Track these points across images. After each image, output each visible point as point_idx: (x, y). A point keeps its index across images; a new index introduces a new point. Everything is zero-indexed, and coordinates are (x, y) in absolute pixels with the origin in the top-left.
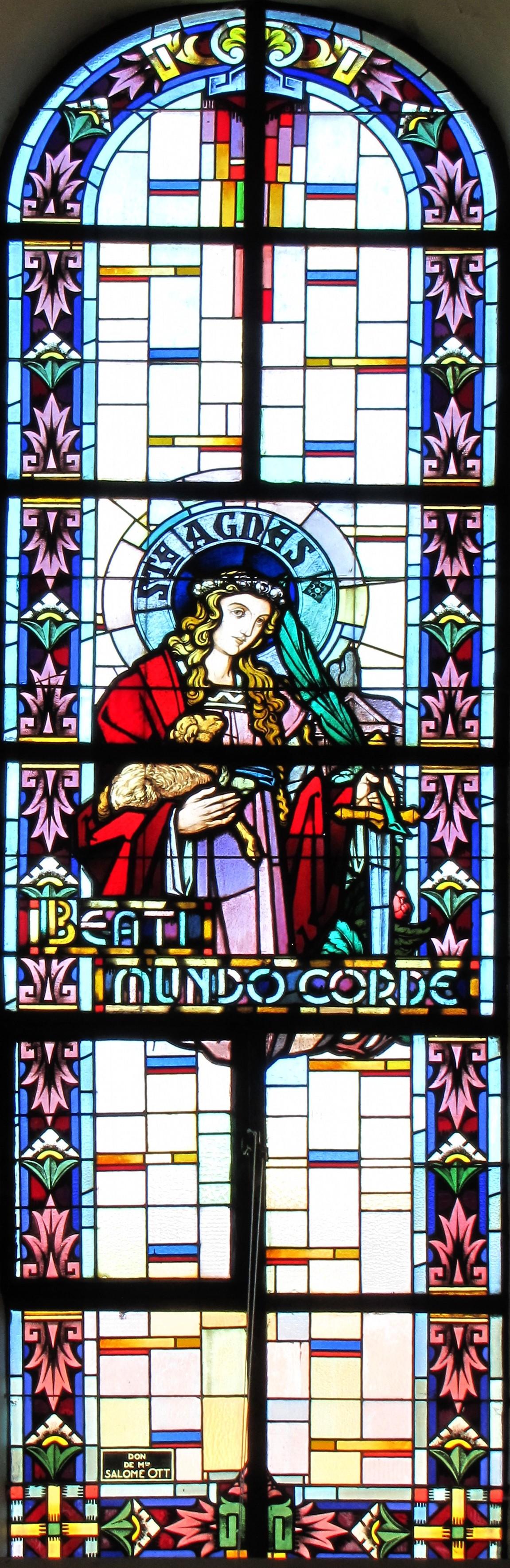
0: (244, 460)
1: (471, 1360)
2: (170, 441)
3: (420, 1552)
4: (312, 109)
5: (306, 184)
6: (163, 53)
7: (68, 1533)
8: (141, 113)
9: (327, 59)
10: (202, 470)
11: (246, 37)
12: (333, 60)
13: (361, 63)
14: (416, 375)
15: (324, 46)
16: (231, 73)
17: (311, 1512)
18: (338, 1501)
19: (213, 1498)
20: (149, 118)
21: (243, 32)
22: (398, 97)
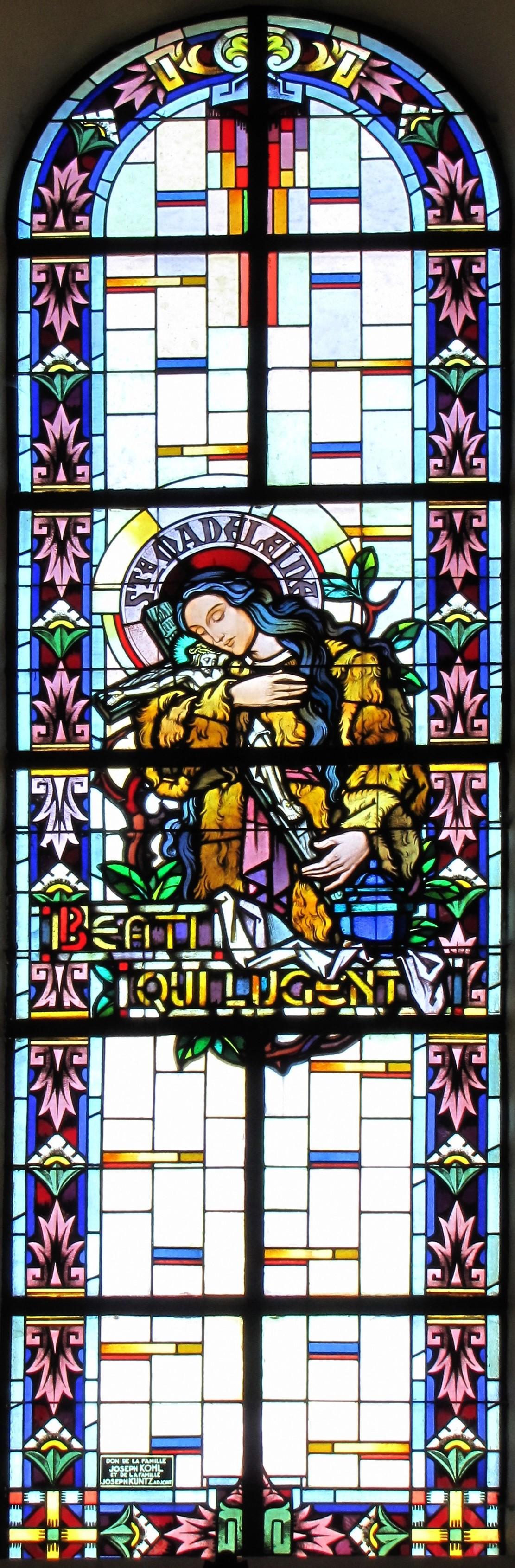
0: (250, 468)
1: (469, 1362)
2: (178, 451)
3: (418, 1552)
4: (312, 113)
6: (166, 64)
7: (66, 1538)
8: (146, 123)
9: (325, 63)
11: (248, 45)
12: (331, 63)
13: (358, 67)
15: (321, 48)
16: (234, 83)
18: (335, 1503)
19: (213, 1505)
20: (155, 129)
21: (246, 41)
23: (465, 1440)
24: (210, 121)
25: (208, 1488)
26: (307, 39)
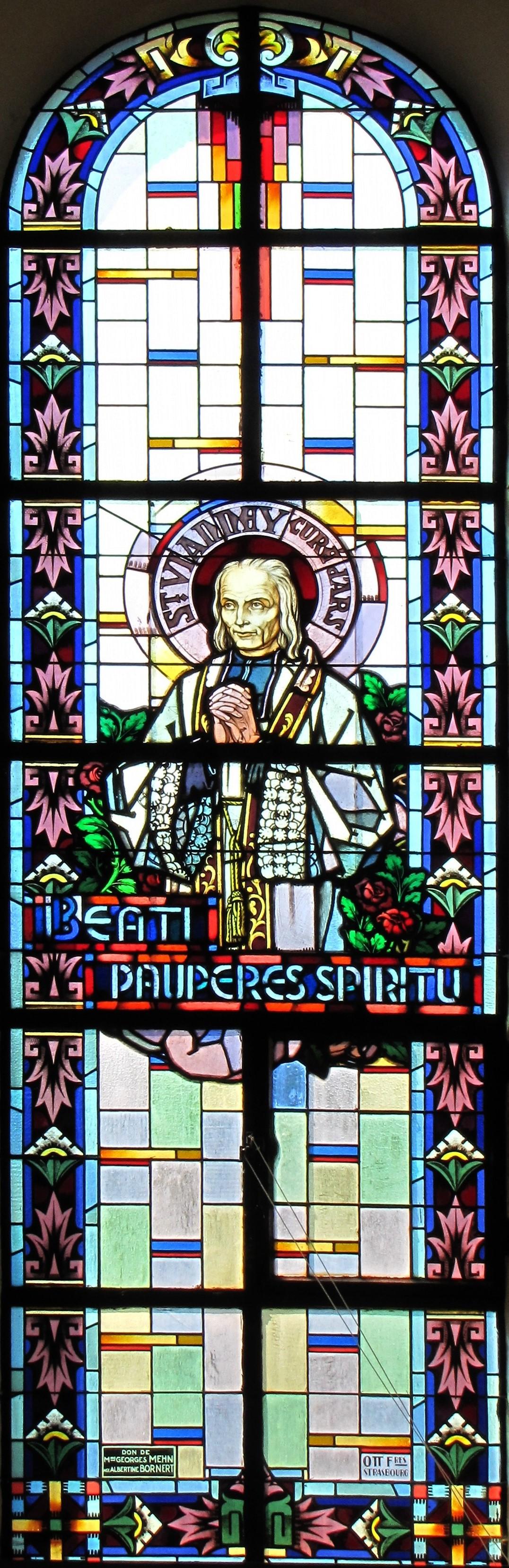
2: (170, 444)
4: (305, 106)
5: (302, 182)
6: (156, 55)
10: (202, 469)
12: (323, 58)
14: (414, 373)
15: (314, 45)
16: (225, 76)
17: (312, 1508)
19: (215, 1496)
20: (145, 120)
22: (389, 94)
23: (460, 613)
24: (200, 113)
25: (211, 1479)
26: (300, 36)
